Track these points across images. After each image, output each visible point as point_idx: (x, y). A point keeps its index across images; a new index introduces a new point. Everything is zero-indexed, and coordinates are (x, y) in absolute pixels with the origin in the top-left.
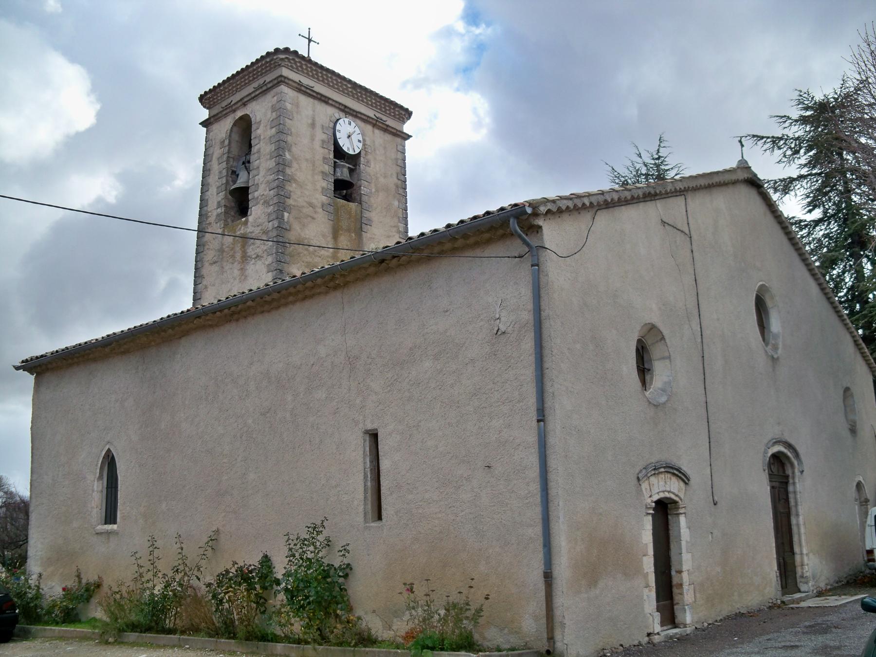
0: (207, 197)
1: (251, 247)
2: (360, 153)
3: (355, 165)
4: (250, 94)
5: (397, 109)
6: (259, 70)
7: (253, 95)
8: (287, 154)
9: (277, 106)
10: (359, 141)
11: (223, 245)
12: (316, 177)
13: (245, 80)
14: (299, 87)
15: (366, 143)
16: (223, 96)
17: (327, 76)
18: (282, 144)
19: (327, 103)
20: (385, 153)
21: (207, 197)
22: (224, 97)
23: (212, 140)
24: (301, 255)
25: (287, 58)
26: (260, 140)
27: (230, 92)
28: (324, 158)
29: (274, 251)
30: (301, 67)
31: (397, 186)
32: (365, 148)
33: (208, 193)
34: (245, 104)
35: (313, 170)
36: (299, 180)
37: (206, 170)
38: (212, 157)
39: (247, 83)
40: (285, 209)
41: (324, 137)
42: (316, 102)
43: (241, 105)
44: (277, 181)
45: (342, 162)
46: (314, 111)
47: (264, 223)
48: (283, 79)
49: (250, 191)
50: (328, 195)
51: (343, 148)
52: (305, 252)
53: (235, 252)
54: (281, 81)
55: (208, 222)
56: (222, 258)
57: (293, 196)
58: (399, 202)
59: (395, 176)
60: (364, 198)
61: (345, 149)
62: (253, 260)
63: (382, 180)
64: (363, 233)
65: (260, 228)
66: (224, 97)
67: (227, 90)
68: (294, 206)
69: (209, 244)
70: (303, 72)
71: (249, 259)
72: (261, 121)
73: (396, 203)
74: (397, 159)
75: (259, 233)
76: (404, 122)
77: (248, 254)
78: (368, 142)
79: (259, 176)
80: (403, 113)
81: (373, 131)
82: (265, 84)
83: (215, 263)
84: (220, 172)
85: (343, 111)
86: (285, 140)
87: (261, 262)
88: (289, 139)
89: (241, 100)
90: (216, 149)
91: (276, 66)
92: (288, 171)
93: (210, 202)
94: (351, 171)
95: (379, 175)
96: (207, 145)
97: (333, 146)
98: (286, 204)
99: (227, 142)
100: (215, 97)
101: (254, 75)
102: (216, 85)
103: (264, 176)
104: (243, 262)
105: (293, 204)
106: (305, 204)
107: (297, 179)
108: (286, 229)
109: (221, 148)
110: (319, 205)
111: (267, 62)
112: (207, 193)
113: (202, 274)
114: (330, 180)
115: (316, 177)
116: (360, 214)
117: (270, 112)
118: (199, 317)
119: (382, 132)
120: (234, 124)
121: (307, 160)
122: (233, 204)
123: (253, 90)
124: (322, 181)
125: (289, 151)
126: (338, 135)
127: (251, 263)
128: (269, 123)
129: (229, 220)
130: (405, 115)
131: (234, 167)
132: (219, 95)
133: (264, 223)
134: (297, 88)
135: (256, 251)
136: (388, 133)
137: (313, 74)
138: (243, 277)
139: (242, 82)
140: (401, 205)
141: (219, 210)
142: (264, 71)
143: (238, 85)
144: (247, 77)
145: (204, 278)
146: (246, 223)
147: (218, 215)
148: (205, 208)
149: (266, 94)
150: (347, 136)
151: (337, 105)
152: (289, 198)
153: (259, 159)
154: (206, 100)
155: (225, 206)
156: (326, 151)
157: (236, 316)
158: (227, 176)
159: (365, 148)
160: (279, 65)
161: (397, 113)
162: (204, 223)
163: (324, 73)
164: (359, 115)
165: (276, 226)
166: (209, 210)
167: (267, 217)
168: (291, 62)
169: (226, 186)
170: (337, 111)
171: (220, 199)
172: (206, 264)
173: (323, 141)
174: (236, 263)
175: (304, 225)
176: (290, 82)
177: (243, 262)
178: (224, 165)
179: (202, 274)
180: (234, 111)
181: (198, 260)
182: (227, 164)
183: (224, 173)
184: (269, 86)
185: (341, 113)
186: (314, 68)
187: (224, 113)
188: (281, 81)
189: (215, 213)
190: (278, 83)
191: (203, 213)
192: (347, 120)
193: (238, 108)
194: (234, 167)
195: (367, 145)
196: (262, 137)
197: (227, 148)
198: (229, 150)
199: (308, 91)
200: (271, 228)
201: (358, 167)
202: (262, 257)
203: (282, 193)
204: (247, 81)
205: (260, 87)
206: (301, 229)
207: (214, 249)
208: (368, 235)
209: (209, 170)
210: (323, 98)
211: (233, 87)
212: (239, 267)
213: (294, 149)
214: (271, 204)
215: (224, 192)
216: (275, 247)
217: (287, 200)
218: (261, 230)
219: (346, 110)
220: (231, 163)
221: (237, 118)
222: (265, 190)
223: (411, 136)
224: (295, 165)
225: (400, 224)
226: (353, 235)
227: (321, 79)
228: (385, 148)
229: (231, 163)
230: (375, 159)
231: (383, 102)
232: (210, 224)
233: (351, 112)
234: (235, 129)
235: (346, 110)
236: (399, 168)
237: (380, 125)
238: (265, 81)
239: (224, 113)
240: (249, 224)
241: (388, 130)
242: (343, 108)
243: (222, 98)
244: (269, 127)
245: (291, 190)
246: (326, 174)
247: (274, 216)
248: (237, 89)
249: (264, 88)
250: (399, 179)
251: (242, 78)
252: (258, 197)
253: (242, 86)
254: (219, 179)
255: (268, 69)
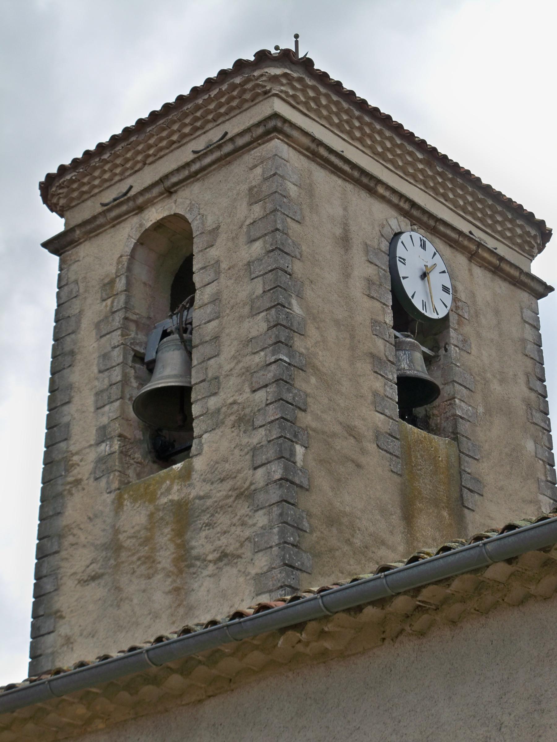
0: (65, 419)
1: (203, 534)
2: (447, 317)
3: (435, 347)
4: (188, 165)
5: (519, 222)
6: (212, 107)
7: (195, 167)
8: (294, 302)
9: (264, 188)
10: (445, 289)
11: (117, 532)
12: (359, 365)
13: (172, 133)
14: (313, 146)
15: (458, 296)
16: (106, 176)
17: (373, 130)
18: (285, 278)
19: (372, 192)
20: (499, 323)
21: (65, 419)
22: (111, 179)
23: (76, 282)
24: (337, 553)
25: (285, 75)
26: (218, 273)
27: (128, 165)
28: (375, 323)
29: (275, 539)
30: (316, 100)
31: (529, 406)
32: (457, 307)
33: (71, 410)
34: (170, 192)
35: (353, 348)
36: (324, 370)
37: (63, 354)
38: (78, 322)
39: (174, 142)
40: (296, 436)
41: (370, 271)
42: (349, 187)
43: (161, 194)
44: (273, 367)
45: (408, 336)
46: (345, 209)
47: (239, 471)
48: (279, 124)
49: (193, 396)
50: (387, 412)
51: (413, 301)
52: (346, 548)
53: (153, 550)
54: (275, 129)
55: (70, 479)
56: (117, 566)
57: (313, 407)
58: (535, 442)
59: (522, 380)
60: (464, 427)
61: (417, 303)
62: (211, 568)
63: (495, 386)
64: (466, 511)
65: (227, 485)
66: (111, 179)
67: (119, 161)
68: (314, 430)
69: (75, 531)
70: (321, 116)
71: (198, 563)
72: (218, 227)
73: (530, 446)
74: (523, 341)
75: (228, 497)
76: (533, 257)
77: (194, 552)
78: (463, 296)
79: (222, 359)
80: (533, 232)
81: (470, 270)
82: (225, 139)
83: (94, 578)
84: (105, 356)
85: (406, 214)
86: (289, 270)
87: (235, 571)
88: (297, 267)
89: (161, 180)
90: (89, 301)
91: (258, 95)
92: (299, 344)
93: (75, 429)
94: (428, 360)
95: (489, 375)
96: (62, 294)
97: (390, 296)
98: (298, 424)
99: (121, 284)
100: (86, 180)
101: (197, 119)
102: (54, 171)
103: (234, 357)
104: (181, 572)
105: (314, 425)
106: (337, 429)
107: (318, 364)
108: (301, 487)
109: (104, 300)
110: (370, 435)
111: (234, 87)
112: (66, 408)
113: (57, 606)
114: (390, 377)
115: (359, 365)
116: (456, 464)
117: (244, 205)
118: (299, 627)
119: (489, 275)
120: (141, 242)
121: (337, 323)
122: (139, 435)
123: (192, 156)
124: (373, 376)
125: (300, 296)
126: (402, 270)
127: (206, 573)
128: (245, 229)
129: (131, 472)
130: (535, 237)
131: (140, 344)
132: (97, 173)
133: (239, 471)
134: (308, 149)
135: (219, 543)
136: (501, 277)
137: (341, 120)
138: (181, 611)
139: (161, 139)
140: (540, 451)
141: (104, 448)
142: (222, 110)
143: (150, 147)
144: (175, 127)
145: (62, 617)
146: (186, 474)
147: (101, 460)
148: (63, 445)
149: (229, 163)
150: (420, 273)
151: (395, 200)
152: (305, 411)
153: (217, 318)
154: (61, 187)
155: (120, 436)
156: (378, 305)
157: (423, 620)
158: (124, 363)
159: (457, 307)
160: (266, 93)
161: (519, 231)
162: (60, 481)
163: (367, 119)
164: (442, 228)
165: (277, 476)
166: (73, 448)
167: (248, 457)
168: (294, 88)
169: (123, 386)
170: (394, 213)
171: (105, 420)
172: (69, 584)
173: (369, 282)
174: (159, 577)
175: (339, 481)
176: (295, 134)
177: (181, 572)
178: (116, 338)
179: (57, 606)
180: (140, 209)
181: (44, 572)
182: (122, 335)
183: (117, 356)
184: (240, 142)
185: (402, 218)
186: (345, 105)
187: (113, 214)
188: (275, 129)
189: (92, 456)
190: (268, 133)
191: (57, 456)
192: (417, 236)
193: (150, 203)
194: (140, 344)
195: (460, 300)
196: (224, 265)
197: (122, 298)
198: (126, 303)
199: (333, 158)
200: (262, 484)
201: (442, 352)
202: (239, 557)
203: (289, 397)
204: (175, 138)
205: (210, 149)
206: (333, 489)
207: (93, 544)
208: (477, 517)
209: (72, 353)
210: (365, 180)
211: (138, 153)
212: (168, 584)
213: (308, 293)
214: (258, 423)
215: (117, 404)
216: (276, 530)
217: (300, 414)
218: (233, 489)
219: (415, 212)
220: (133, 335)
221: (148, 224)
222: (240, 391)
223: (551, 289)
224: (312, 331)
225: (541, 497)
226: (445, 514)
227: (358, 134)
228: (497, 312)
229: (133, 335)
230: (479, 335)
231: (490, 202)
232: (78, 482)
233: (425, 219)
234: (141, 253)
235: (415, 212)
236: (529, 363)
237: (486, 255)
238: (226, 133)
239: (113, 214)
240: (195, 476)
241: (502, 270)
242: (406, 206)
243: (106, 181)
244: (243, 239)
245: (309, 391)
246: (379, 359)
247: (271, 453)
248: (149, 156)
249: (229, 148)
250: (531, 389)
251: (163, 129)
252: (218, 411)
253: (161, 149)
254: (100, 372)
255: (234, 103)
